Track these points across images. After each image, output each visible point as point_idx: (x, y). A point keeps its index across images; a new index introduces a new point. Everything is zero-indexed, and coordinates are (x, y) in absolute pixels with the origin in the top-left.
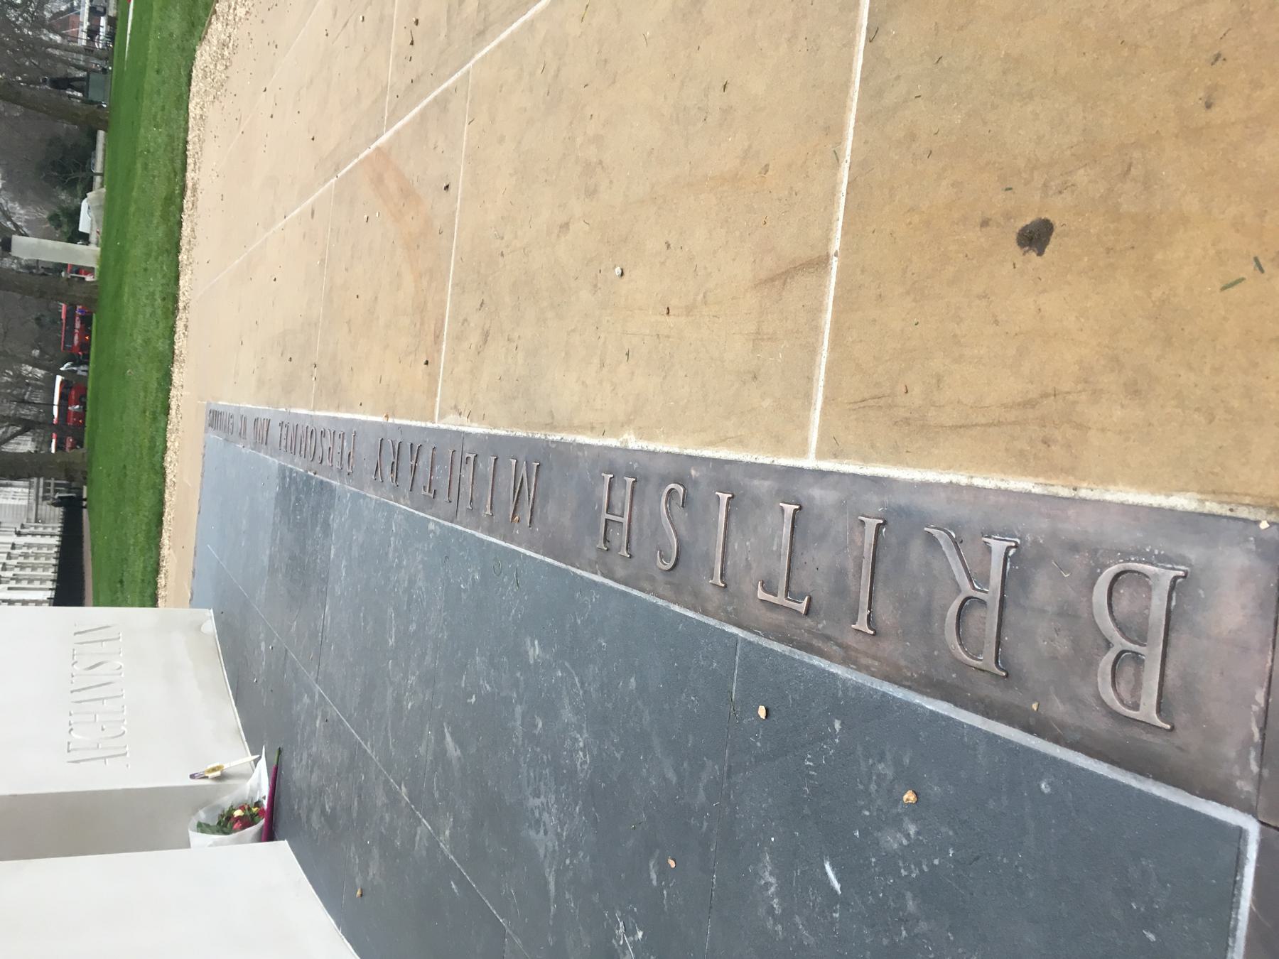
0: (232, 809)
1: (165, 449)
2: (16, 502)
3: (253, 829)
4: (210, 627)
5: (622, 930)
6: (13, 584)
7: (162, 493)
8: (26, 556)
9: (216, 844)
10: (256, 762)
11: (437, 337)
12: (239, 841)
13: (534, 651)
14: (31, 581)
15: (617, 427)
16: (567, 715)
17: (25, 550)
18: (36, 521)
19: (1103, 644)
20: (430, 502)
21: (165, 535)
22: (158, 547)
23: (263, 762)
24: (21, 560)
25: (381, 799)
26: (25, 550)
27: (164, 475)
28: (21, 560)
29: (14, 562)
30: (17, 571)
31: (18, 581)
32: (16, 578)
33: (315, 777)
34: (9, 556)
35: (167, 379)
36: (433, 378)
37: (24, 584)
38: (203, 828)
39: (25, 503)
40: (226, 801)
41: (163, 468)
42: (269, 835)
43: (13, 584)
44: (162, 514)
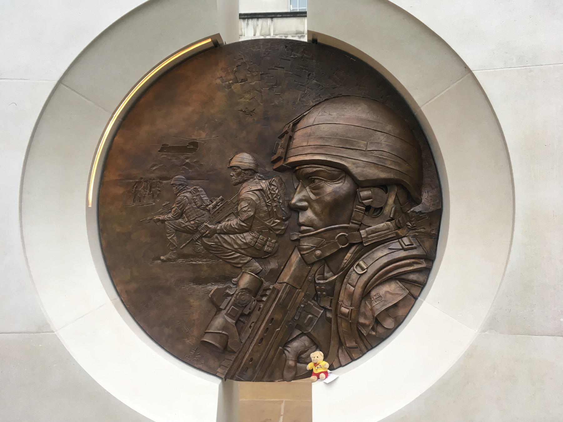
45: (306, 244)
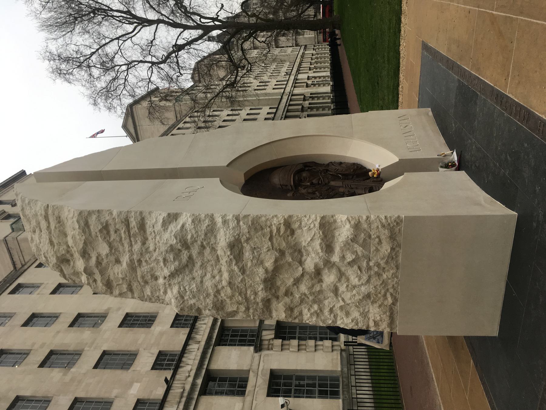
0: (448, 163)
1: (400, 45)
2: (310, 36)
3: (454, 168)
4: (431, 113)
5: (311, 75)
6: (315, 70)
7: (399, 60)
8: (317, 58)
9: (446, 171)
10: (452, 153)
11: (508, 75)
12: (451, 170)
13: (526, 145)
14: (320, 68)
15: (542, 114)
16: (531, 156)
17: (316, 56)
18: (318, 43)
19: (97, 291)
20: (506, 110)
21: (401, 75)
22: (398, 78)
23: (455, 153)
24: (316, 60)
25: (492, 165)
26: (316, 56)
27: (399, 54)
28: (316, 60)
29: (313, 61)
30: (315, 65)
31: (316, 69)
32: (315, 68)
33: (473, 158)
34: (312, 59)
35: (399, 21)
36: (507, 83)
37: (318, 70)
38: (442, 167)
39: (313, 36)
40: (446, 161)
41: (399, 52)
42: (458, 169)
43: (315, 70)
44: (399, 67)
45: (327, 181)
